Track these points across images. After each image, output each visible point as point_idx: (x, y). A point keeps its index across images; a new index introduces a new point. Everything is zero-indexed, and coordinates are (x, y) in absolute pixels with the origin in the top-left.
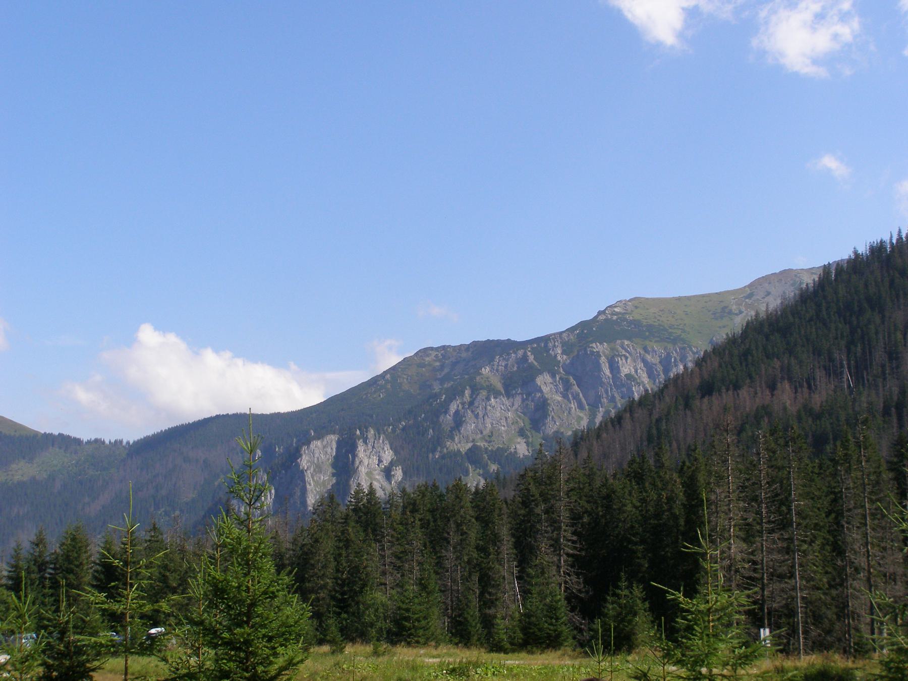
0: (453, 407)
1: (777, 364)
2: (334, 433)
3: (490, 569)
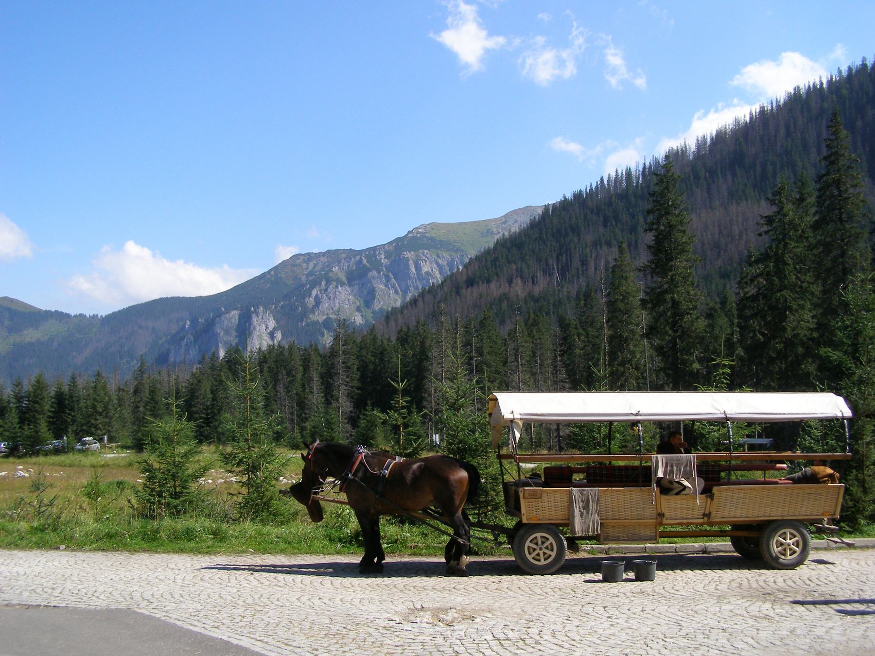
0: (314, 292)
1: (514, 266)
2: (236, 309)
3: (306, 398)
